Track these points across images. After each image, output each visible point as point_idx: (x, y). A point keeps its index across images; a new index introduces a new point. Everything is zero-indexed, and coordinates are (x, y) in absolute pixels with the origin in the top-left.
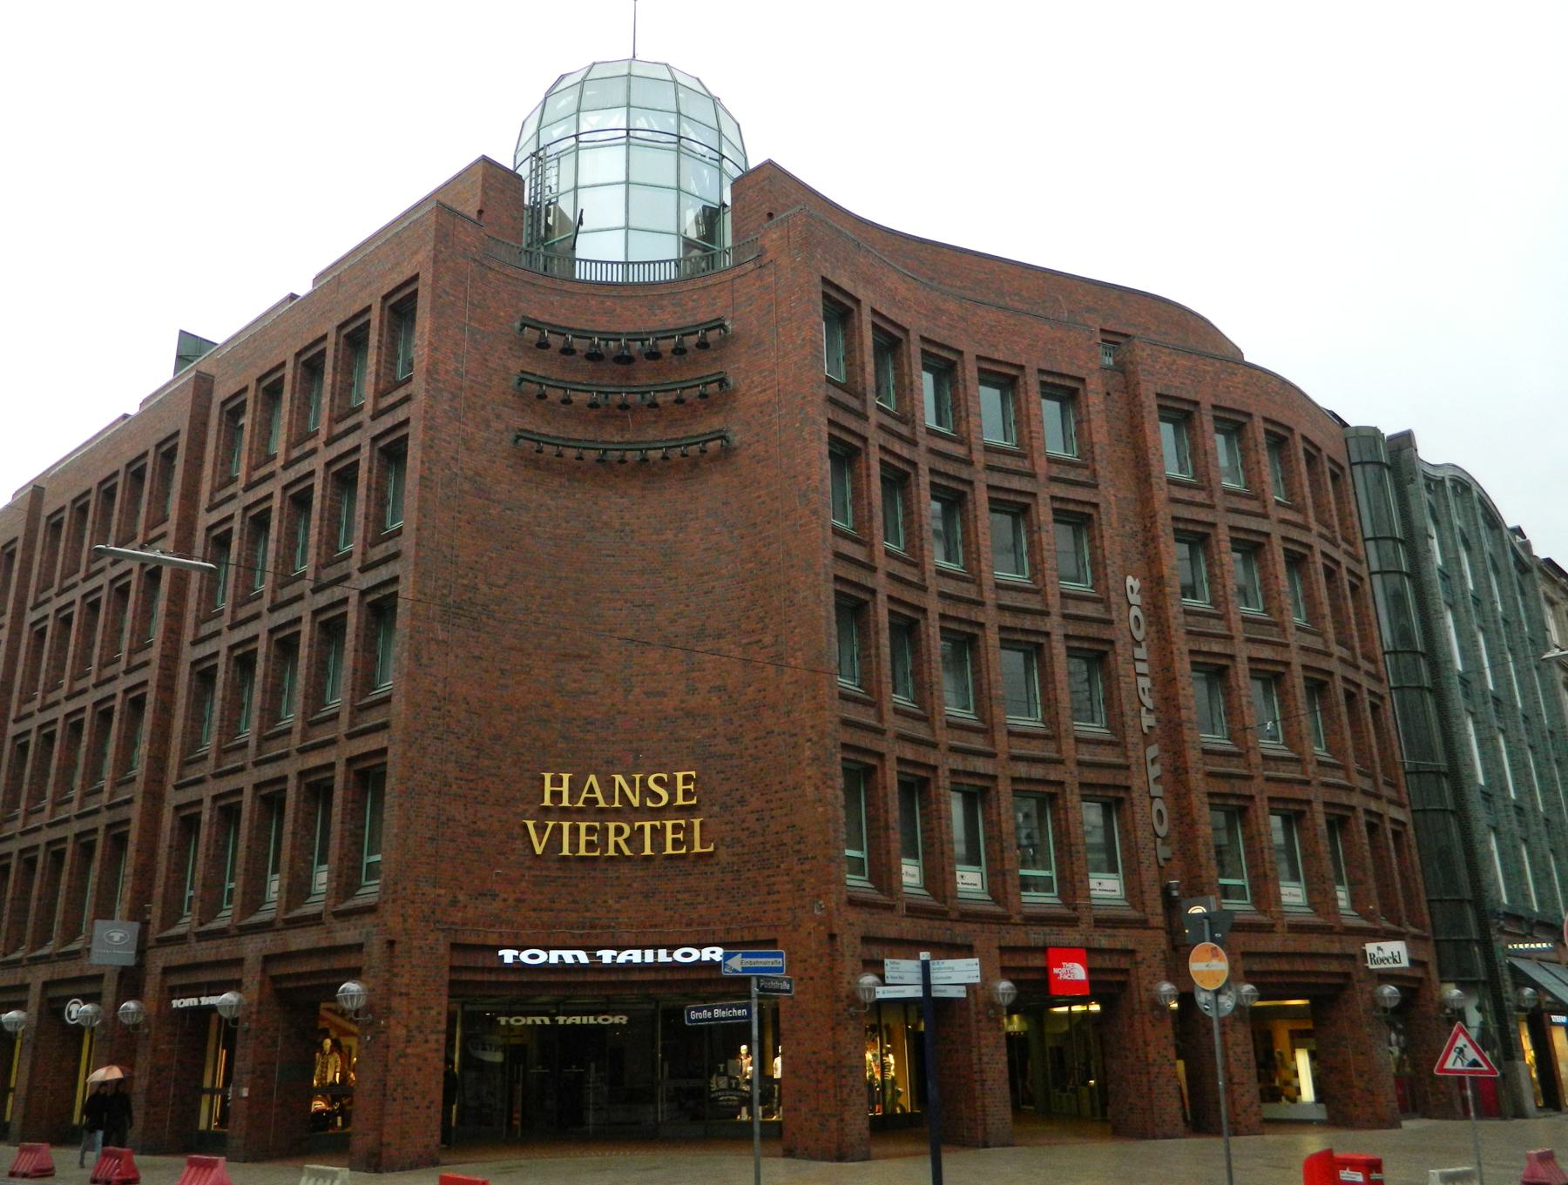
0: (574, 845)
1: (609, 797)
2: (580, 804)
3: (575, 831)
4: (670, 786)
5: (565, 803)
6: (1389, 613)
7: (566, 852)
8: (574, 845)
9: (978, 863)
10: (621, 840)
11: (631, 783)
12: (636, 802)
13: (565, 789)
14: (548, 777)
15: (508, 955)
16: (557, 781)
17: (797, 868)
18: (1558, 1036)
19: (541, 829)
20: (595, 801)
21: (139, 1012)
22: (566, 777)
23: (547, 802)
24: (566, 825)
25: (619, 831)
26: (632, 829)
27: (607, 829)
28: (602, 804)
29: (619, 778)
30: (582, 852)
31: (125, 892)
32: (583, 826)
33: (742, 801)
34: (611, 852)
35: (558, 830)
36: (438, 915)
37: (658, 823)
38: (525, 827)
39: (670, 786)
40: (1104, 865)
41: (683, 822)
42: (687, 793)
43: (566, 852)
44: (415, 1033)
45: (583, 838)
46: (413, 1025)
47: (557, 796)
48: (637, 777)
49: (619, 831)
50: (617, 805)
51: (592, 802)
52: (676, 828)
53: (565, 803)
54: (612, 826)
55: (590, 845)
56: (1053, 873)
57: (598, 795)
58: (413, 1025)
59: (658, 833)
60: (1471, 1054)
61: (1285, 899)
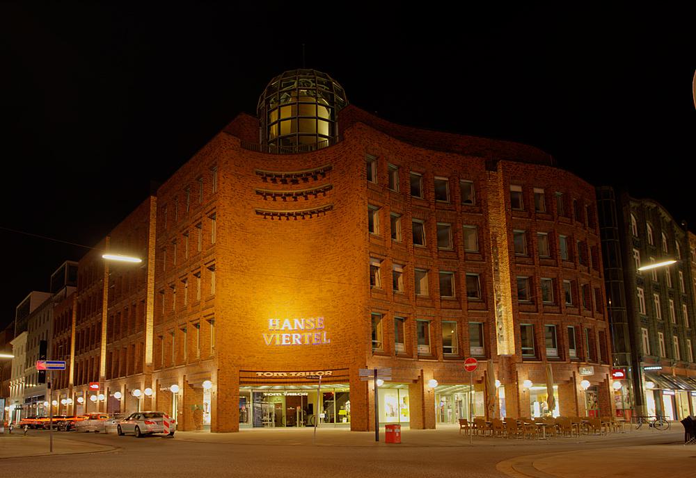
0: (281, 341)
1: (293, 326)
3: (281, 336)
6: (650, 264)
9: (428, 344)
10: (297, 339)
11: (300, 322)
15: (260, 374)
17: (356, 346)
18: (693, 398)
19: (269, 336)
21: (682, 383)
24: (278, 336)
25: (296, 337)
28: (290, 328)
31: (587, 352)
33: (338, 326)
34: (294, 343)
36: (234, 362)
37: (310, 334)
40: (552, 346)
41: (289, 335)
44: (229, 396)
46: (228, 393)
48: (302, 319)
49: (296, 337)
52: (287, 336)
54: (294, 335)
55: (287, 341)
56: (533, 349)
58: (228, 393)
60: (271, 406)
61: (570, 355)
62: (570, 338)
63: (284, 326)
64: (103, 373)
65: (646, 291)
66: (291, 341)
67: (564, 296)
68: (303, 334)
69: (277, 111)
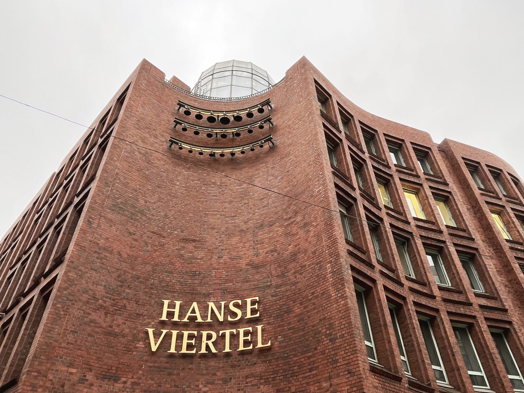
0: (179, 347)
1: (204, 317)
2: (186, 320)
3: (180, 337)
4: (242, 307)
5: (176, 319)
7: (173, 350)
8: (179, 347)
10: (210, 343)
11: (219, 308)
12: (221, 318)
13: (177, 311)
14: (166, 302)
16: (172, 306)
19: (157, 335)
20: (196, 318)
22: (178, 303)
23: (164, 318)
24: (175, 333)
25: (209, 337)
26: (218, 336)
27: (201, 336)
28: (200, 320)
29: (211, 305)
30: (184, 351)
32: (186, 333)
34: (203, 351)
35: (169, 336)
37: (234, 331)
38: (147, 333)
39: (242, 307)
41: (195, 333)
42: (253, 311)
43: (173, 350)
45: (185, 341)
47: (170, 315)
48: (223, 303)
49: (209, 337)
50: (209, 320)
51: (193, 319)
52: (190, 337)
53: (176, 319)
54: (205, 333)
55: (190, 347)
57: (198, 314)
59: (234, 337)
62: (370, 203)
63: (189, 314)
64: (394, 310)
65: (96, 206)
66: (255, 343)
67: (403, 282)
68: (221, 332)
69: (211, 82)
